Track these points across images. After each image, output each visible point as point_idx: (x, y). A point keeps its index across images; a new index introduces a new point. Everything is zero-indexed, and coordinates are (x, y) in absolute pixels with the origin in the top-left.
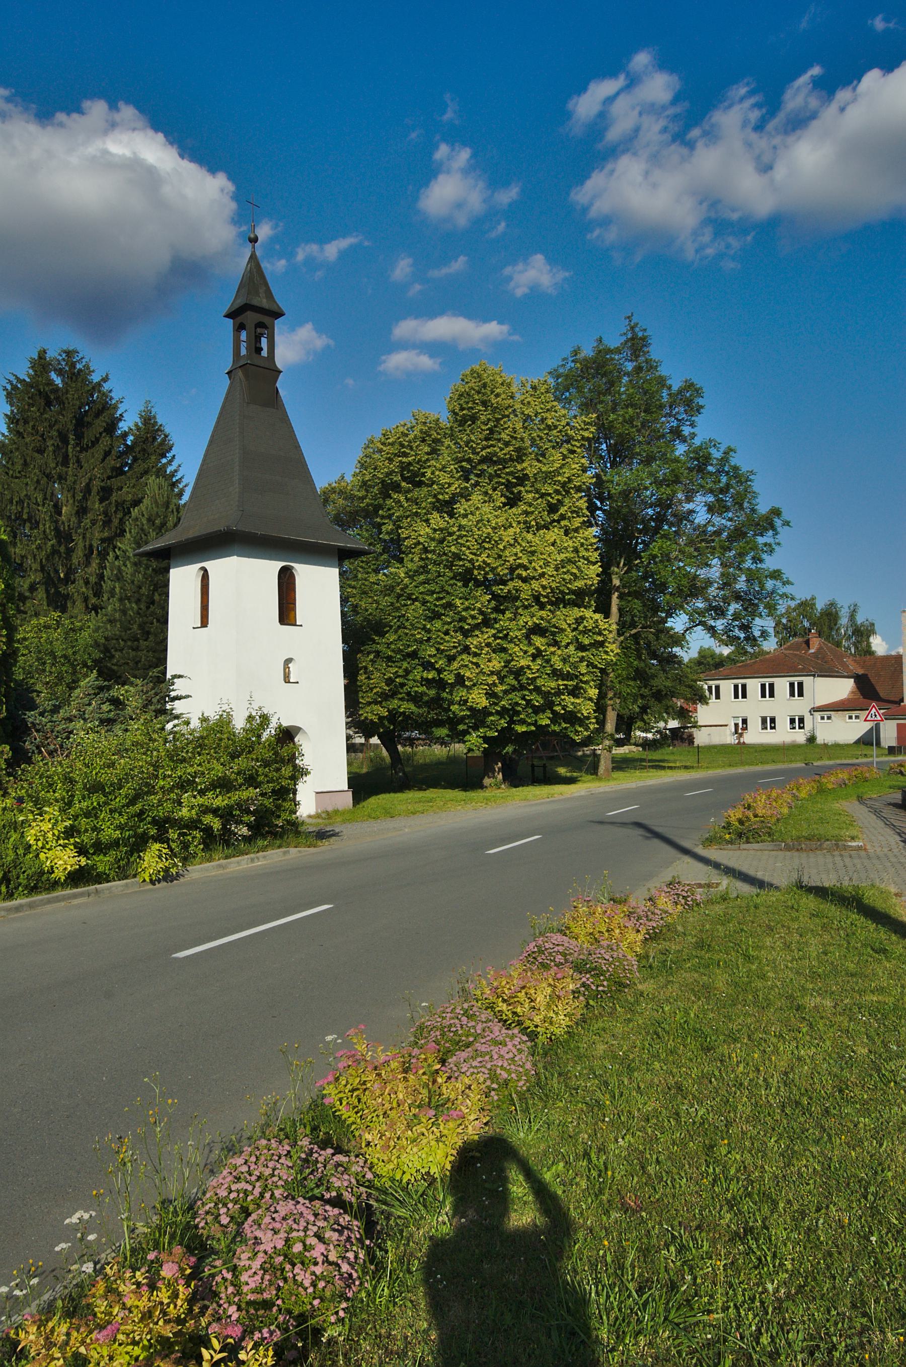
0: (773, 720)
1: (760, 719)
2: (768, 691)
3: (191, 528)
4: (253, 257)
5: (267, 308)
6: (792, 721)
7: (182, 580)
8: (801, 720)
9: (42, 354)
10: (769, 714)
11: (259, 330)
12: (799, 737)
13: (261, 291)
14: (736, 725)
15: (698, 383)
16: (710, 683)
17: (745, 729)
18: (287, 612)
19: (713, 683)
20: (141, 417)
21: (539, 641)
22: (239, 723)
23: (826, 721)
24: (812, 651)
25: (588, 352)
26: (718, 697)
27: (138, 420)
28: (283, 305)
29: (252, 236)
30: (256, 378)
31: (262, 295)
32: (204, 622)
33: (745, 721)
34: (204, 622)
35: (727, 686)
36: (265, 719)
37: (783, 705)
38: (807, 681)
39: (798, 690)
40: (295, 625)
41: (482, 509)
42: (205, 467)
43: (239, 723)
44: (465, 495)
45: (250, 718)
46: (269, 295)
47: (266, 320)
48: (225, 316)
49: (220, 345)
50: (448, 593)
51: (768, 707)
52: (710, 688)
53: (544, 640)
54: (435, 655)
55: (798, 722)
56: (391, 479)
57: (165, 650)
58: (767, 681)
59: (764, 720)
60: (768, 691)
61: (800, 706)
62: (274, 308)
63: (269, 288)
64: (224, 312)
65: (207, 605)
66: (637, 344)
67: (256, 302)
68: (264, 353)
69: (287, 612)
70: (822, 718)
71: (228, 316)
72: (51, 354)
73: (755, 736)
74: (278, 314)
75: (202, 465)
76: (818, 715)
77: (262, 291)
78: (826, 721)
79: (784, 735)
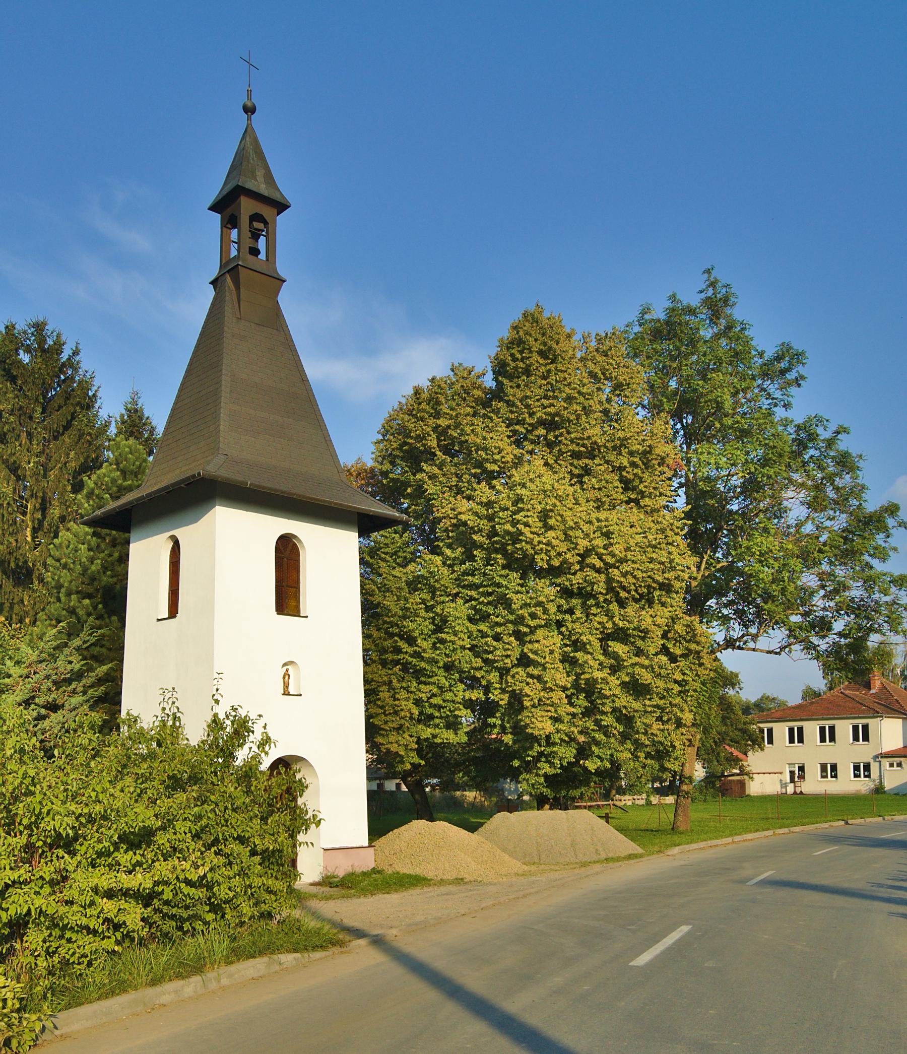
0: (834, 767)
1: (819, 766)
2: (828, 735)
3: (158, 478)
4: (248, 131)
5: (266, 194)
6: (856, 768)
7: (147, 555)
8: (867, 767)
9: (10, 328)
10: (829, 760)
11: (257, 225)
12: (863, 785)
13: (258, 173)
14: (792, 773)
15: (797, 346)
16: (761, 725)
17: (802, 777)
18: (287, 598)
19: (765, 726)
20: (127, 410)
21: (618, 647)
22: (194, 732)
23: (895, 768)
24: (873, 691)
25: (659, 313)
26: (771, 741)
27: (124, 412)
28: (286, 189)
29: (249, 104)
30: (246, 285)
31: (260, 173)
32: (173, 611)
33: (802, 769)
34: (173, 611)
35: (781, 730)
36: (242, 728)
37: (846, 751)
38: (872, 723)
39: (862, 734)
40: (299, 616)
41: (539, 477)
42: (179, 405)
43: (194, 732)
44: (518, 462)
45: (216, 724)
46: (269, 178)
47: (266, 211)
48: (210, 209)
49: (204, 243)
50: (499, 585)
51: (829, 753)
52: (762, 731)
53: (626, 648)
54: (481, 668)
55: (861, 769)
56: (423, 445)
57: (122, 648)
58: (827, 724)
59: (824, 767)
60: (828, 735)
61: (864, 752)
62: (275, 196)
63: (269, 171)
64: (208, 205)
65: (177, 590)
66: (716, 306)
67: (250, 185)
68: (262, 256)
69: (287, 598)
70: (891, 765)
71: (214, 208)
72: (21, 326)
73: (813, 784)
74: (281, 207)
75: (176, 403)
76: (886, 763)
77: (260, 173)
78: (895, 768)
79: (847, 783)
